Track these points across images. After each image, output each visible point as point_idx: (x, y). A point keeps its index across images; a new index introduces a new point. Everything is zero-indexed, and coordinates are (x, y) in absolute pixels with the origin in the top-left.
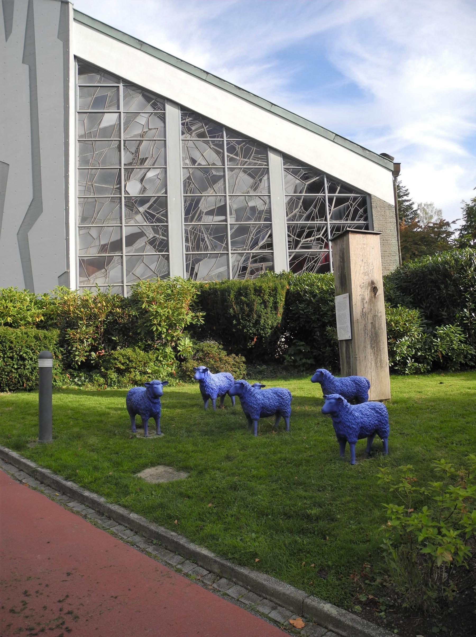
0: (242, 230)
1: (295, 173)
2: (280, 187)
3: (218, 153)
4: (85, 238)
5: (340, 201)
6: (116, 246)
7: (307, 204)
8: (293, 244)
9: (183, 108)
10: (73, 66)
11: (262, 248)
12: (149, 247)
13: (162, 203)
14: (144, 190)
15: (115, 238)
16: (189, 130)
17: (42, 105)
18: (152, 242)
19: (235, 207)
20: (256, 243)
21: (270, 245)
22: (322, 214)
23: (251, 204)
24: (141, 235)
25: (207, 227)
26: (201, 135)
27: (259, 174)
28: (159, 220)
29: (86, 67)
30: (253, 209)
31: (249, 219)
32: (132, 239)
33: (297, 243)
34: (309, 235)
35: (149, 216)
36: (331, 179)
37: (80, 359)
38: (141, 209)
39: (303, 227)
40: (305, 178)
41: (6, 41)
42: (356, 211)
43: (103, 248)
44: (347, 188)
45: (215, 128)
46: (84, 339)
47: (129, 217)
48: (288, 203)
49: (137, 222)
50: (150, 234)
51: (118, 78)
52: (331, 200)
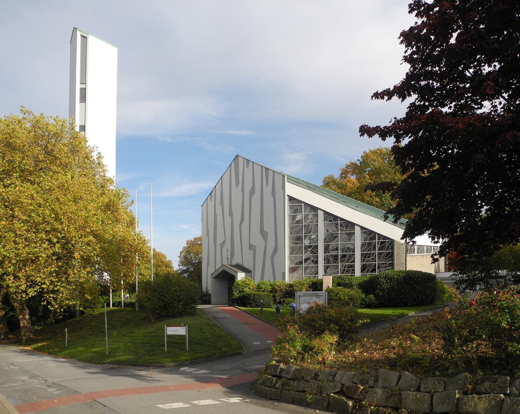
0: (344, 256)
1: (365, 233)
2: (358, 239)
3: (336, 227)
4: (291, 260)
5: (382, 243)
6: (301, 263)
7: (369, 244)
8: (363, 260)
9: (324, 211)
10: (287, 198)
11: (351, 262)
12: (312, 263)
13: (316, 247)
14: (310, 243)
15: (300, 260)
16: (326, 219)
17: (217, 250)
18: (313, 261)
19: (342, 247)
20: (348, 261)
21: (354, 261)
22: (374, 248)
23: (347, 246)
24: (309, 259)
25: (331, 255)
26: (331, 221)
27: (351, 235)
28: (315, 253)
29: (291, 199)
30: (348, 248)
31: (346, 252)
32: (306, 260)
33: (364, 260)
34: (369, 257)
35: (312, 252)
36: (379, 234)
37: (278, 301)
38: (309, 250)
39: (367, 254)
40: (369, 235)
41: (377, 95)
42: (388, 247)
43: (297, 264)
44: (385, 238)
45: (336, 218)
46: (278, 295)
47: (305, 252)
48: (361, 245)
49: (309, 254)
50: (312, 259)
51: (302, 202)
52: (378, 243)
